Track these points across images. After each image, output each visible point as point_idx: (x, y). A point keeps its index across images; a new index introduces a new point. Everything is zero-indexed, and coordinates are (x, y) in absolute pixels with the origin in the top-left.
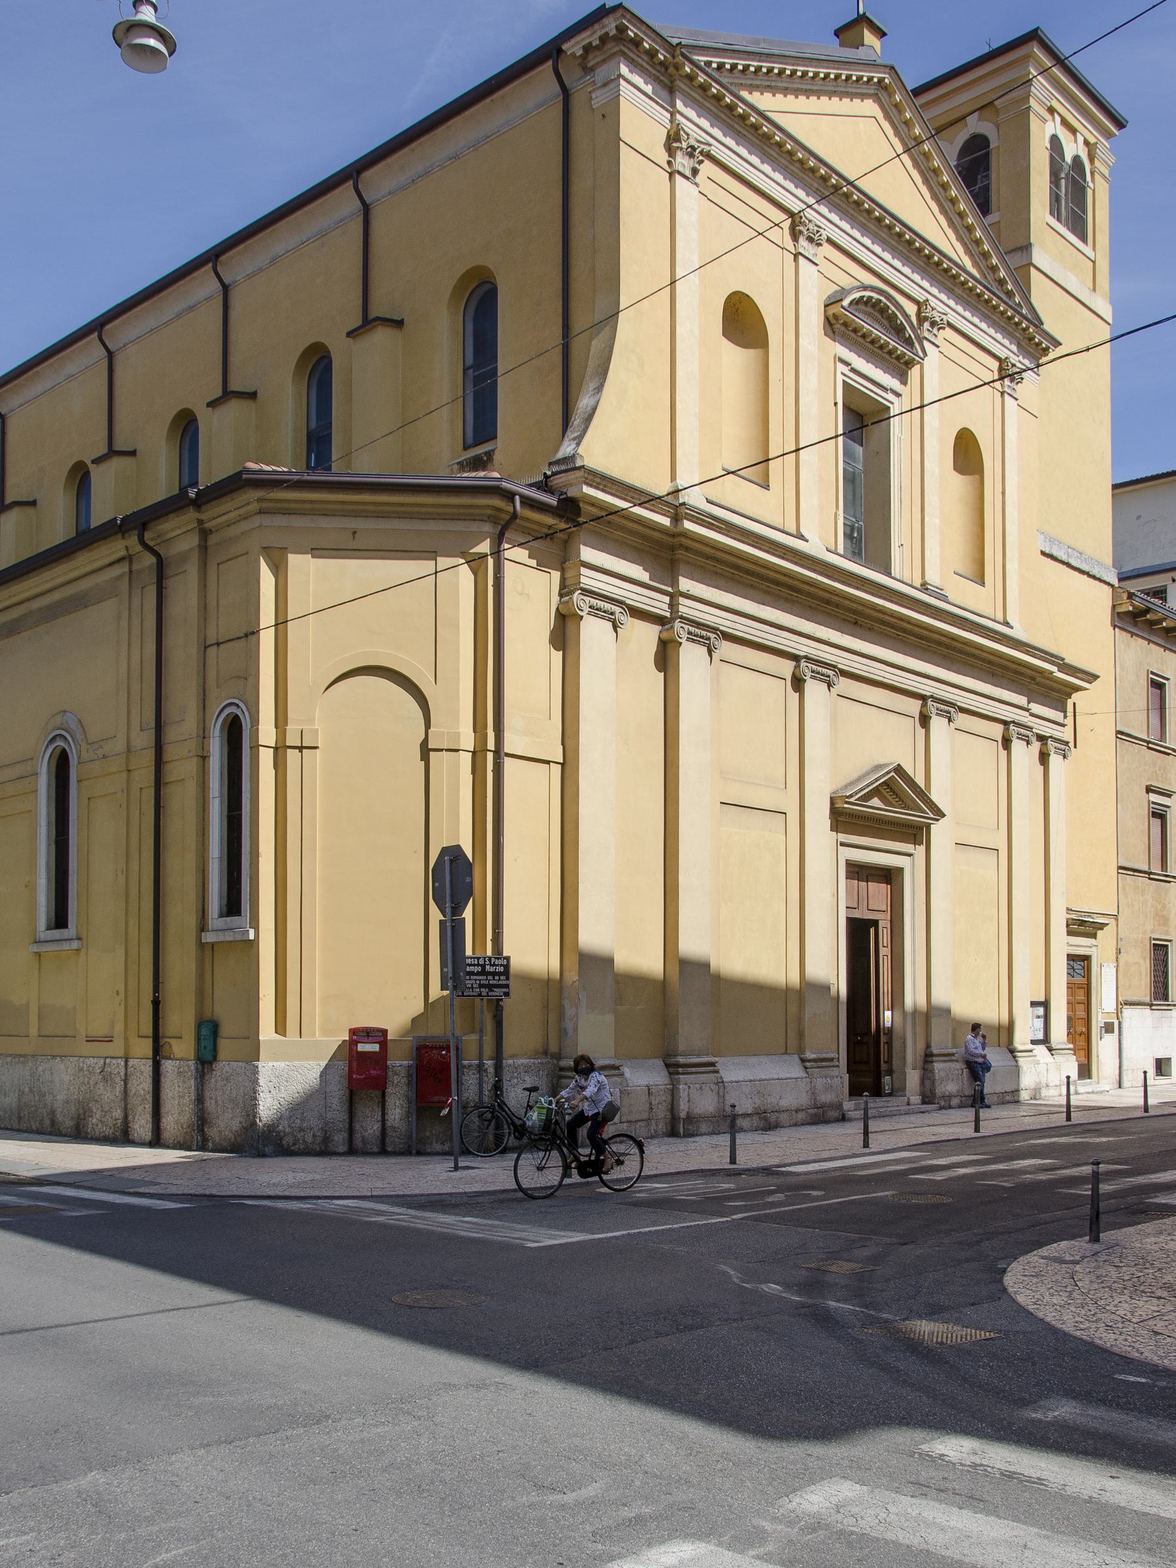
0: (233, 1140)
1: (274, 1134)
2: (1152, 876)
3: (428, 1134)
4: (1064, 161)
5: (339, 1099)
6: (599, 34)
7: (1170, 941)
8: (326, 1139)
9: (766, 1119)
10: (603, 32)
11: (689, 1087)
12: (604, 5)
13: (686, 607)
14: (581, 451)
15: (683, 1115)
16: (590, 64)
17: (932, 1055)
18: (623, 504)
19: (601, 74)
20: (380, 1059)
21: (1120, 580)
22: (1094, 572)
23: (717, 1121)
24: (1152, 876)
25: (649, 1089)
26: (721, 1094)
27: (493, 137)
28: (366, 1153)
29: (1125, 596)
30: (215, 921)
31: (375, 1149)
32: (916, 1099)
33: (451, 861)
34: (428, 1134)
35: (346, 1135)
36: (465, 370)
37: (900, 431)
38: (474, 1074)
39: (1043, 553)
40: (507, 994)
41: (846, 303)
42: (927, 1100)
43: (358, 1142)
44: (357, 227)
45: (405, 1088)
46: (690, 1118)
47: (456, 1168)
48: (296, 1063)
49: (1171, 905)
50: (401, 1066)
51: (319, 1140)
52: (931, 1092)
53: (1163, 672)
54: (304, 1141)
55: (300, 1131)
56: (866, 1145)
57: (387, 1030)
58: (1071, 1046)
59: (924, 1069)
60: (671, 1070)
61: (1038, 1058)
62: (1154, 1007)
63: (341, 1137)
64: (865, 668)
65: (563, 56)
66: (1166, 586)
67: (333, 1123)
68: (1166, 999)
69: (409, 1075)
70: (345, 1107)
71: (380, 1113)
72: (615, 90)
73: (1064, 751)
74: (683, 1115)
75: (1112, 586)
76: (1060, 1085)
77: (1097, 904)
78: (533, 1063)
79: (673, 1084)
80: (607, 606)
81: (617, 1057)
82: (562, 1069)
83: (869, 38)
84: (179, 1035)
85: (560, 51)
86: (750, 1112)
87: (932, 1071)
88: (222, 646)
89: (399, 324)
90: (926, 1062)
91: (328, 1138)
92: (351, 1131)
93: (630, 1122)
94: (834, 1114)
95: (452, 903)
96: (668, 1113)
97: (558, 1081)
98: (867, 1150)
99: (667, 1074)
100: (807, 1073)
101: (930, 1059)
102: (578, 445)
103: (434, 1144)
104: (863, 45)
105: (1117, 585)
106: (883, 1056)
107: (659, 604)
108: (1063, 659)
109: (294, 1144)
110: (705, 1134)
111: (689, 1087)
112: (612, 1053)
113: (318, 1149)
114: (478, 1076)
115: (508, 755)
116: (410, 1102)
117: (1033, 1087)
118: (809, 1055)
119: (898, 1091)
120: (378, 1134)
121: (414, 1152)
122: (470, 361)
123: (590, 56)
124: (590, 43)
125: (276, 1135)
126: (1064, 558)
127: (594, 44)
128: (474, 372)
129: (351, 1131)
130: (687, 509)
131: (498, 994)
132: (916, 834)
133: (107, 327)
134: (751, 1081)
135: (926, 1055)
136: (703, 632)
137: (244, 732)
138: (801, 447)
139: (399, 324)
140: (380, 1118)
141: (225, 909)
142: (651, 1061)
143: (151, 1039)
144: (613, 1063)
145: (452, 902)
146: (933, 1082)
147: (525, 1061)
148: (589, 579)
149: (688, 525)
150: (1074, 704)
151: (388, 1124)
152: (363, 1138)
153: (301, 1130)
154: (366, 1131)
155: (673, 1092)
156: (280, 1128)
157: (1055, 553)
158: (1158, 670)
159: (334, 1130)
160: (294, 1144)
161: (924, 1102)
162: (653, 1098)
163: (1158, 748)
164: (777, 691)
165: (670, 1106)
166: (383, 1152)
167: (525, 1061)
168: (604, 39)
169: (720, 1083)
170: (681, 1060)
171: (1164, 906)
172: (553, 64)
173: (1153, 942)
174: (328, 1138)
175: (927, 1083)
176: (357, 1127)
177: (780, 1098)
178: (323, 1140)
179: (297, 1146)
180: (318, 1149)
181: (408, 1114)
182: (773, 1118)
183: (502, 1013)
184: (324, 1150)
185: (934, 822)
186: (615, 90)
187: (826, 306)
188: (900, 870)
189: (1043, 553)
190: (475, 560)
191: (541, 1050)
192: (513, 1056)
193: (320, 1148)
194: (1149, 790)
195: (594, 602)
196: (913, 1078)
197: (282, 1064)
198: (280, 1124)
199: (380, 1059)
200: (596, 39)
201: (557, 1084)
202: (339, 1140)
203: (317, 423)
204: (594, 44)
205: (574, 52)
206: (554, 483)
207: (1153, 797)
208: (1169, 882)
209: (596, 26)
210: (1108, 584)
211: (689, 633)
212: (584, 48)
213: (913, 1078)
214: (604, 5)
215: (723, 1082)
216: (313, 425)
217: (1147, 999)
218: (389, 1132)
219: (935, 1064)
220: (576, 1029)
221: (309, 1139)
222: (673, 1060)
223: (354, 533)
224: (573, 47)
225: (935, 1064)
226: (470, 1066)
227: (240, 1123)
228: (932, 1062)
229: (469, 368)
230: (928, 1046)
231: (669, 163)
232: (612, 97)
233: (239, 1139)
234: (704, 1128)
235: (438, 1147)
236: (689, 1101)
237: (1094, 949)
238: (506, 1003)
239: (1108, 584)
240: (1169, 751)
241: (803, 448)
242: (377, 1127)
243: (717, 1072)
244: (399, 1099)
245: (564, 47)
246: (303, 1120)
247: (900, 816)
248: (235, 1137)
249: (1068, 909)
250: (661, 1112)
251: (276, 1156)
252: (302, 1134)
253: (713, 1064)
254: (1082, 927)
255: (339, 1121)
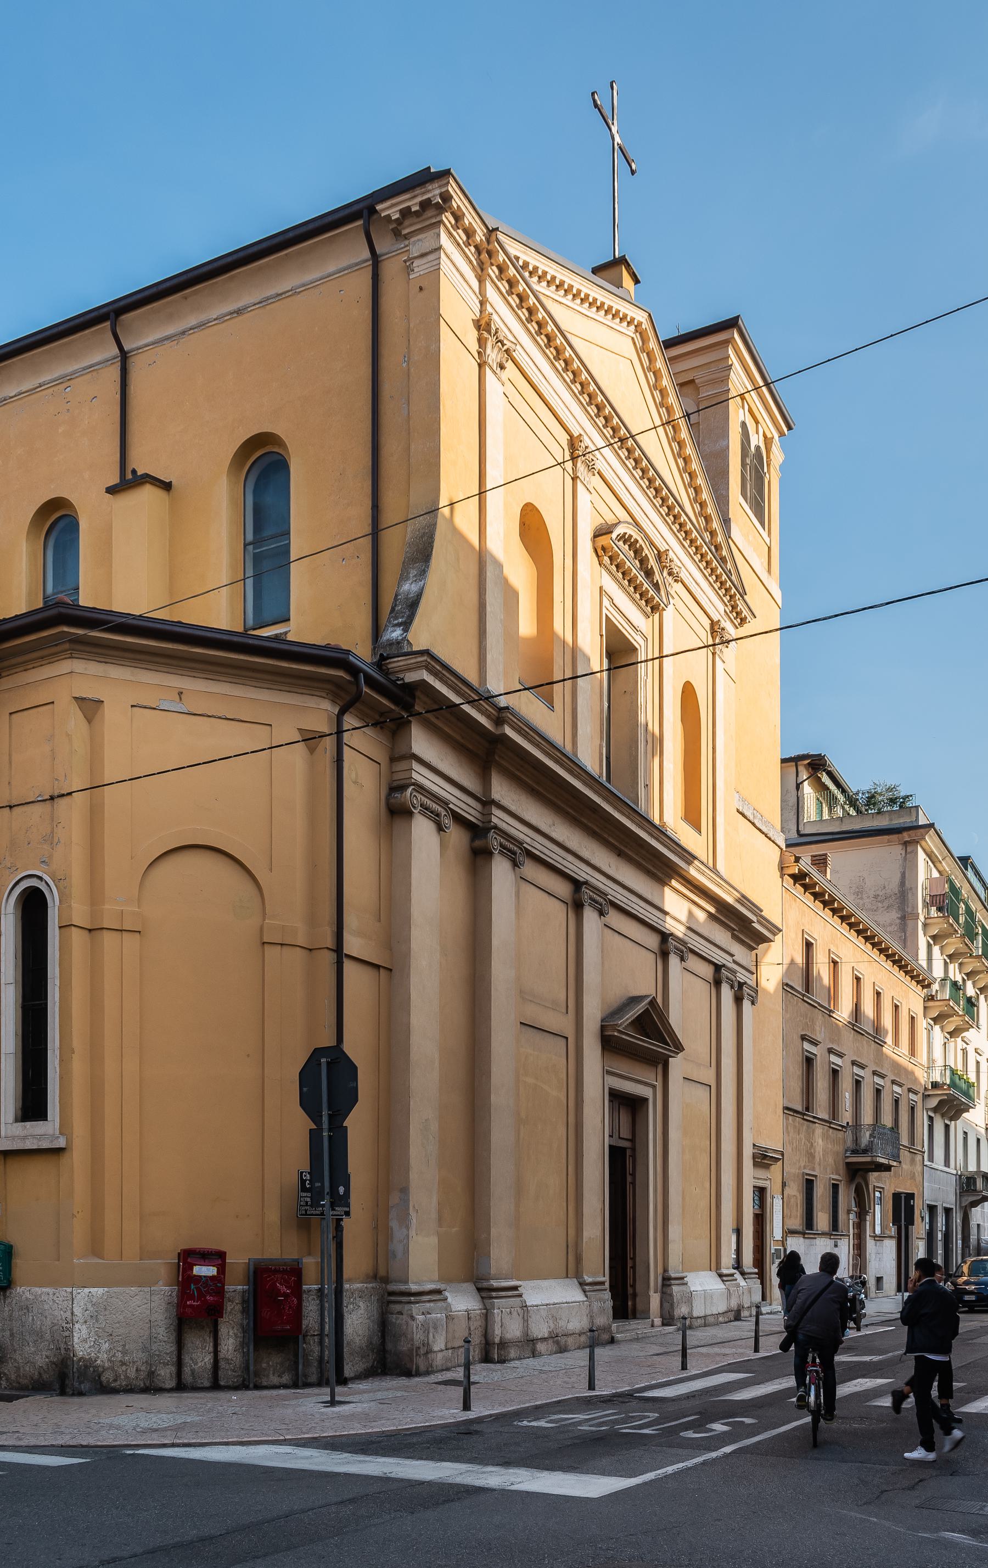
0: (36, 1377)
1: (91, 1369)
2: (805, 1117)
3: (264, 1365)
4: (750, 449)
5: (166, 1329)
6: (419, 199)
7: (816, 1176)
8: (151, 1374)
9: (558, 1343)
10: (425, 197)
11: (502, 1311)
12: (429, 168)
13: (498, 818)
14: (410, 636)
15: (497, 1340)
16: (405, 232)
17: (670, 1279)
18: (456, 700)
19: (418, 245)
20: (217, 1284)
21: (788, 846)
22: (770, 835)
23: (523, 1346)
24: (805, 1117)
25: (468, 1314)
26: (526, 1318)
27: (284, 296)
28: (195, 1389)
29: (793, 859)
30: (9, 1126)
31: (207, 1384)
32: (658, 1321)
33: (328, 1063)
34: (264, 1365)
35: (173, 1369)
36: (245, 545)
37: (645, 674)
38: (314, 1299)
39: (738, 811)
40: (347, 1214)
41: (614, 535)
42: (665, 1321)
43: (187, 1377)
44: (114, 372)
45: (239, 1316)
46: (503, 1344)
47: (333, 1403)
48: (115, 1289)
49: (816, 1144)
50: (235, 1291)
51: (143, 1375)
52: (670, 1315)
53: (812, 932)
54: (127, 1377)
55: (122, 1365)
56: (684, 1367)
57: (225, 1253)
58: (756, 1270)
59: (663, 1293)
60: (484, 1294)
61: (738, 1281)
62: (806, 1236)
63: (168, 1371)
64: (625, 900)
65: (375, 217)
66: (826, 855)
67: (158, 1356)
68: (837, 1230)
69: (244, 1301)
70: (173, 1337)
71: (211, 1344)
72: (435, 263)
73: (752, 997)
74: (497, 1340)
75: (782, 849)
76: (751, 1307)
77: (773, 1141)
78: (366, 1288)
79: (486, 1309)
80: (435, 806)
81: (441, 1279)
82: (391, 1294)
83: (627, 281)
84: (687, 1082)
85: (372, 211)
86: (546, 1336)
87: (671, 1295)
88: (17, 811)
89: (167, 486)
90: (663, 1285)
91: (153, 1373)
92: (179, 1364)
93: (454, 1348)
94: (606, 1337)
95: (329, 1110)
96: (483, 1339)
97: (388, 1305)
98: (685, 1374)
99: (480, 1298)
100: (586, 1296)
101: (668, 1283)
102: (406, 630)
103: (271, 1376)
104: (622, 287)
105: (784, 849)
106: (630, 1281)
107: (469, 809)
108: (762, 911)
109: (115, 1380)
110: (514, 1359)
111: (502, 1311)
112: (436, 1277)
113: (142, 1385)
114: (318, 1302)
115: (348, 956)
116: (244, 1332)
117: (736, 1309)
118: (589, 1279)
119: (646, 1314)
120: (209, 1366)
121: (251, 1385)
122: (250, 537)
123: (407, 223)
124: (409, 208)
125: (94, 1371)
126: (751, 818)
127: (413, 210)
128: (254, 549)
129: (179, 1364)
130: (510, 713)
131: (339, 1213)
132: (661, 1063)
133: (123, 317)
134: (547, 1305)
135: (664, 1279)
136: (511, 846)
137: (49, 910)
138: (664, 655)
139: (167, 486)
140: (211, 1349)
141: (20, 1113)
142: (465, 1285)
143: (279, 1257)
144: (439, 1287)
145: (329, 1109)
146: (672, 1305)
147: (359, 1285)
148: (421, 775)
149: (509, 731)
150: (757, 954)
151: (221, 1355)
152: (193, 1371)
153: (123, 1363)
154: (196, 1364)
155: (487, 1316)
156: (99, 1362)
157: (746, 813)
158: (809, 931)
159: (160, 1363)
160: (115, 1380)
161: (663, 1324)
162: (471, 1323)
163: (809, 1001)
164: (557, 913)
165: (484, 1331)
166: (216, 1386)
167: (359, 1285)
168: (426, 205)
169: (524, 1306)
170: (495, 1284)
171: (812, 1144)
172: (111, 324)
173: (806, 1177)
174: (153, 1373)
175: (666, 1305)
176: (186, 1359)
177: (568, 1322)
178: (148, 1375)
179: (119, 1383)
180: (142, 1385)
181: (243, 1344)
182: (562, 1340)
183: (342, 1234)
184: (151, 1388)
185: (674, 1055)
186: (435, 263)
187: (595, 536)
188: (644, 1100)
189: (738, 811)
190: (315, 738)
191: (371, 1274)
192: (350, 1281)
193: (144, 1384)
194: (803, 1038)
195: (425, 800)
196: (655, 1300)
197: (100, 1291)
198: (98, 1357)
199: (217, 1284)
200: (416, 204)
201: (386, 1309)
202: (166, 1374)
203: (53, 589)
204: (413, 210)
205: (389, 215)
206: (390, 666)
207: (807, 1046)
208: (815, 1123)
209: (418, 191)
210: (779, 847)
211: (501, 845)
212: (401, 211)
213: (655, 1300)
214: (429, 168)
215: (526, 1306)
216: (50, 590)
217: (799, 1228)
218: (222, 1364)
219: (674, 1287)
220: (406, 1251)
221: (132, 1373)
222: (485, 1284)
223: (180, 694)
224: (390, 210)
225: (674, 1287)
226: (309, 1291)
227: (47, 1357)
228: (670, 1285)
229: (250, 544)
230: (665, 1270)
231: (479, 353)
232: (432, 269)
233: (45, 1376)
234: (513, 1353)
235: (275, 1380)
236: (501, 1326)
237: (768, 1182)
238: (346, 1222)
239: (779, 847)
240: (816, 1005)
241: (777, 630)
242: (208, 1359)
243: (520, 1296)
244: (233, 1328)
245: (378, 207)
246: (124, 1353)
247: (652, 1047)
248: (40, 1374)
249: (754, 1145)
250: (477, 1339)
251: (96, 1394)
252: (124, 1368)
253: (515, 1288)
254: (763, 1159)
255: (167, 1354)
